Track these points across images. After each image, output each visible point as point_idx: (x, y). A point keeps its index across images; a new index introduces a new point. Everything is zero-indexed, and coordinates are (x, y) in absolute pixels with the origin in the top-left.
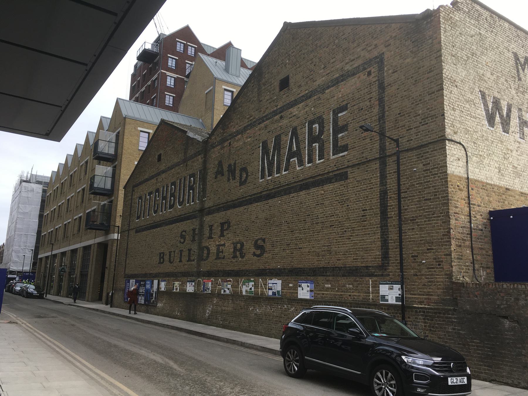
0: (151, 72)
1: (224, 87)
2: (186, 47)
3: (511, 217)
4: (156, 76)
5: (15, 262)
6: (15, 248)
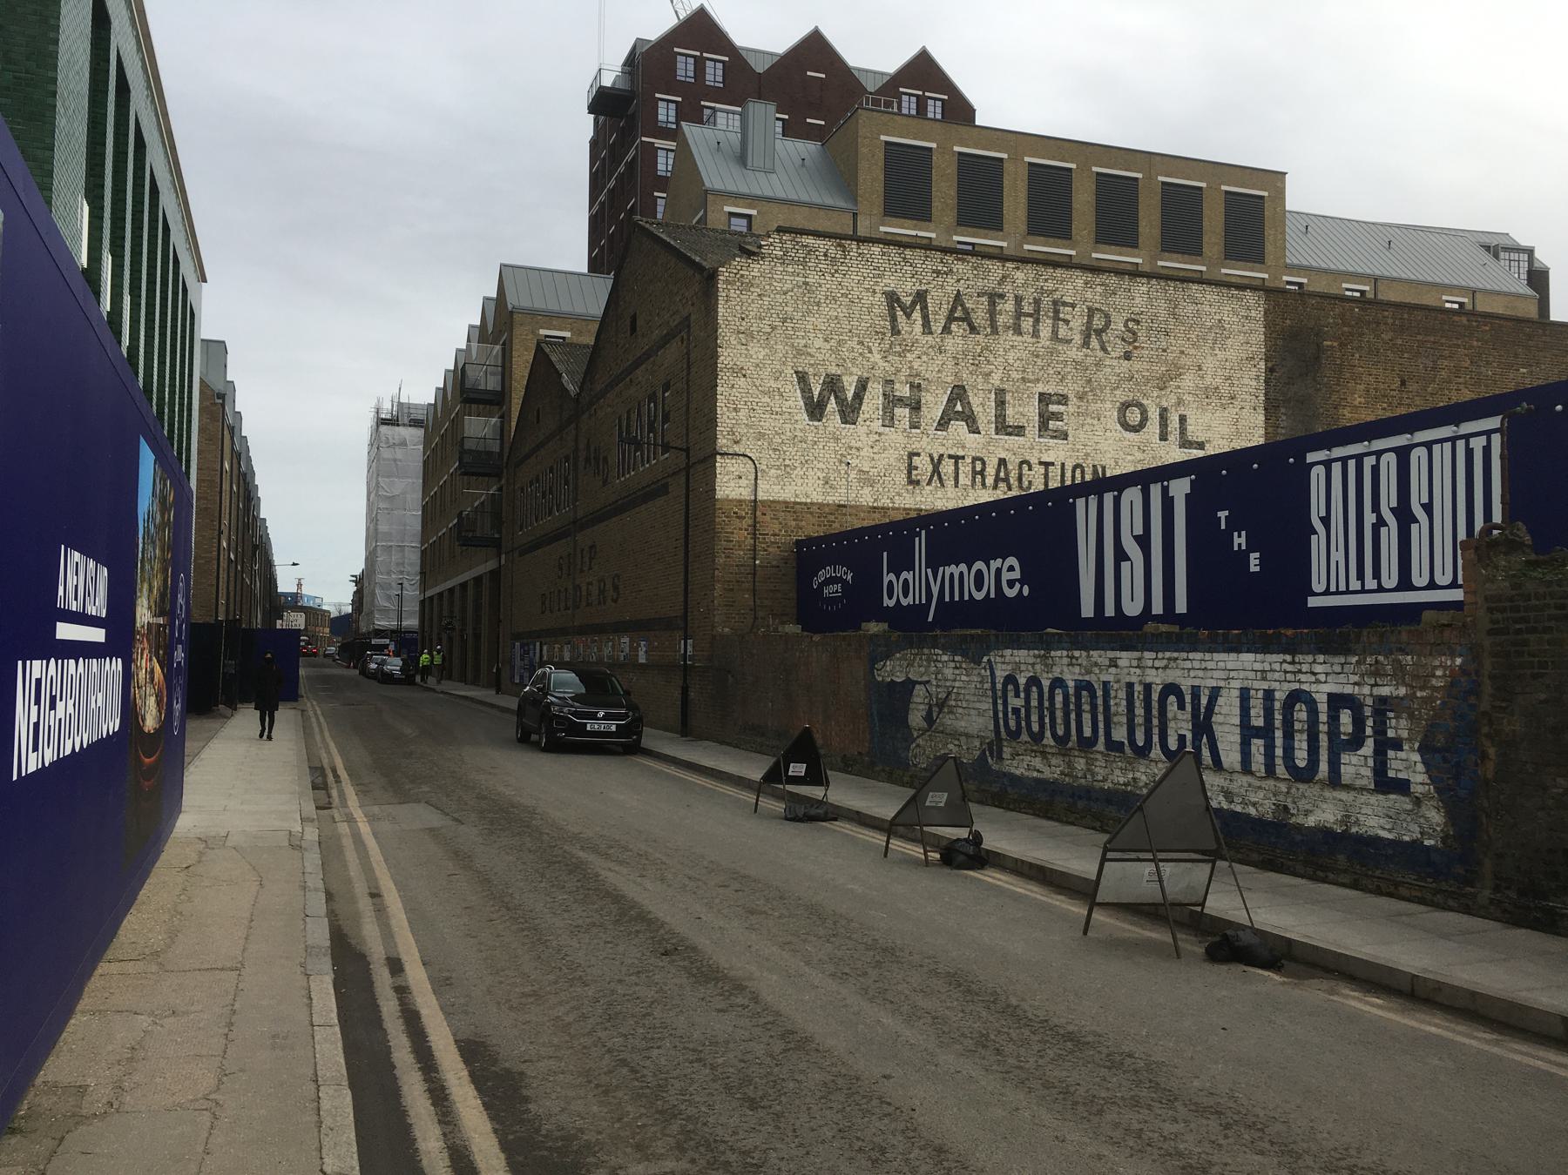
0: (627, 135)
1: (727, 209)
2: (700, 64)
3: (1559, 408)
4: (632, 153)
5: (385, 611)
6: (380, 577)
